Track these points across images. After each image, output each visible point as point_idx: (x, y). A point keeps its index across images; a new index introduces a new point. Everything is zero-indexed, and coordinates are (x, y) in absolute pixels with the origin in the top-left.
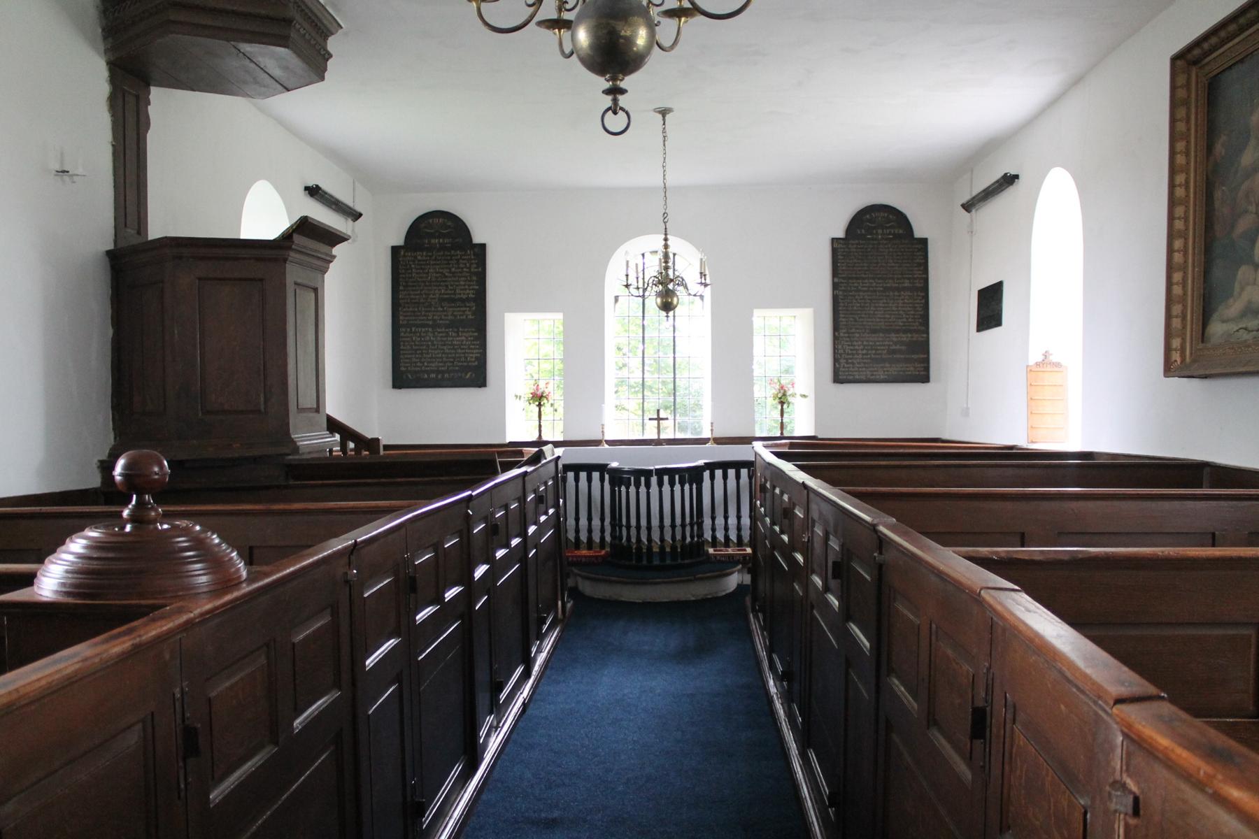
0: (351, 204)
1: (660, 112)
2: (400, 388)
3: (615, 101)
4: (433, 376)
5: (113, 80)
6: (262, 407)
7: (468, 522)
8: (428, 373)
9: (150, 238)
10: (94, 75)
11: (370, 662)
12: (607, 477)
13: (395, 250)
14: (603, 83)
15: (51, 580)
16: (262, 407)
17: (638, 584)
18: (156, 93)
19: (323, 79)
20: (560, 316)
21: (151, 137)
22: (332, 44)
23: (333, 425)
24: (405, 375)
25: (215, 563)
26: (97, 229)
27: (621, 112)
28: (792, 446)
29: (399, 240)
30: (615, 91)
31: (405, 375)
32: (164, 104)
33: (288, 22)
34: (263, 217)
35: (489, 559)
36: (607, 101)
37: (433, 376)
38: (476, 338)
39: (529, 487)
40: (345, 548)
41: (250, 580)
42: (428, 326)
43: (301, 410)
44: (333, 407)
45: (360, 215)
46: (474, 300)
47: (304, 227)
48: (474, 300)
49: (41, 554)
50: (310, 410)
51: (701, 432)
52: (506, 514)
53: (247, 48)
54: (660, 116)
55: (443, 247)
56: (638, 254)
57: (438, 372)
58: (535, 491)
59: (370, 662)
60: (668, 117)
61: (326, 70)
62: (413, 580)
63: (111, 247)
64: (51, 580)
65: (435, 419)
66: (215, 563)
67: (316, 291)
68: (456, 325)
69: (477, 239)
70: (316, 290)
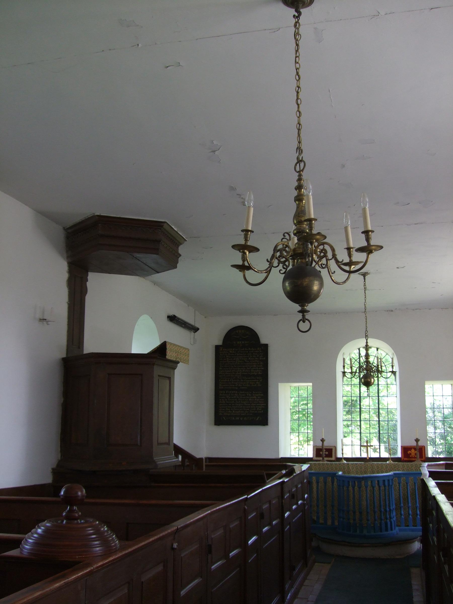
0: (192, 323)
1: (362, 275)
3: (303, 316)
4: (238, 418)
5: (70, 271)
6: (139, 444)
7: (246, 513)
9: (84, 353)
10: (60, 269)
11: (183, 592)
12: (336, 480)
13: (217, 347)
14: (297, 307)
15: (29, 542)
16: (139, 444)
18: (91, 276)
19: (176, 267)
20: (311, 384)
21: (88, 298)
22: (181, 250)
23: (178, 450)
24: (222, 418)
25: (105, 542)
26: (60, 351)
27: (306, 321)
28: (447, 466)
29: (219, 342)
30: (303, 311)
31: (222, 418)
32: (96, 282)
33: (159, 241)
34: (142, 343)
35: (258, 532)
36: (300, 316)
37: (238, 418)
39: (286, 489)
40: (172, 532)
41: (122, 548)
43: (159, 444)
44: (177, 440)
45: (198, 329)
47: (161, 350)
49: (27, 529)
50: (165, 444)
51: (395, 453)
52: (297, 490)
53: (138, 255)
54: (362, 277)
56: (351, 353)
58: (289, 492)
59: (183, 592)
60: (366, 277)
61: (178, 263)
62: (210, 547)
63: (64, 356)
64: (29, 542)
65: (239, 443)
66: (105, 542)
67: (170, 379)
70: (169, 378)
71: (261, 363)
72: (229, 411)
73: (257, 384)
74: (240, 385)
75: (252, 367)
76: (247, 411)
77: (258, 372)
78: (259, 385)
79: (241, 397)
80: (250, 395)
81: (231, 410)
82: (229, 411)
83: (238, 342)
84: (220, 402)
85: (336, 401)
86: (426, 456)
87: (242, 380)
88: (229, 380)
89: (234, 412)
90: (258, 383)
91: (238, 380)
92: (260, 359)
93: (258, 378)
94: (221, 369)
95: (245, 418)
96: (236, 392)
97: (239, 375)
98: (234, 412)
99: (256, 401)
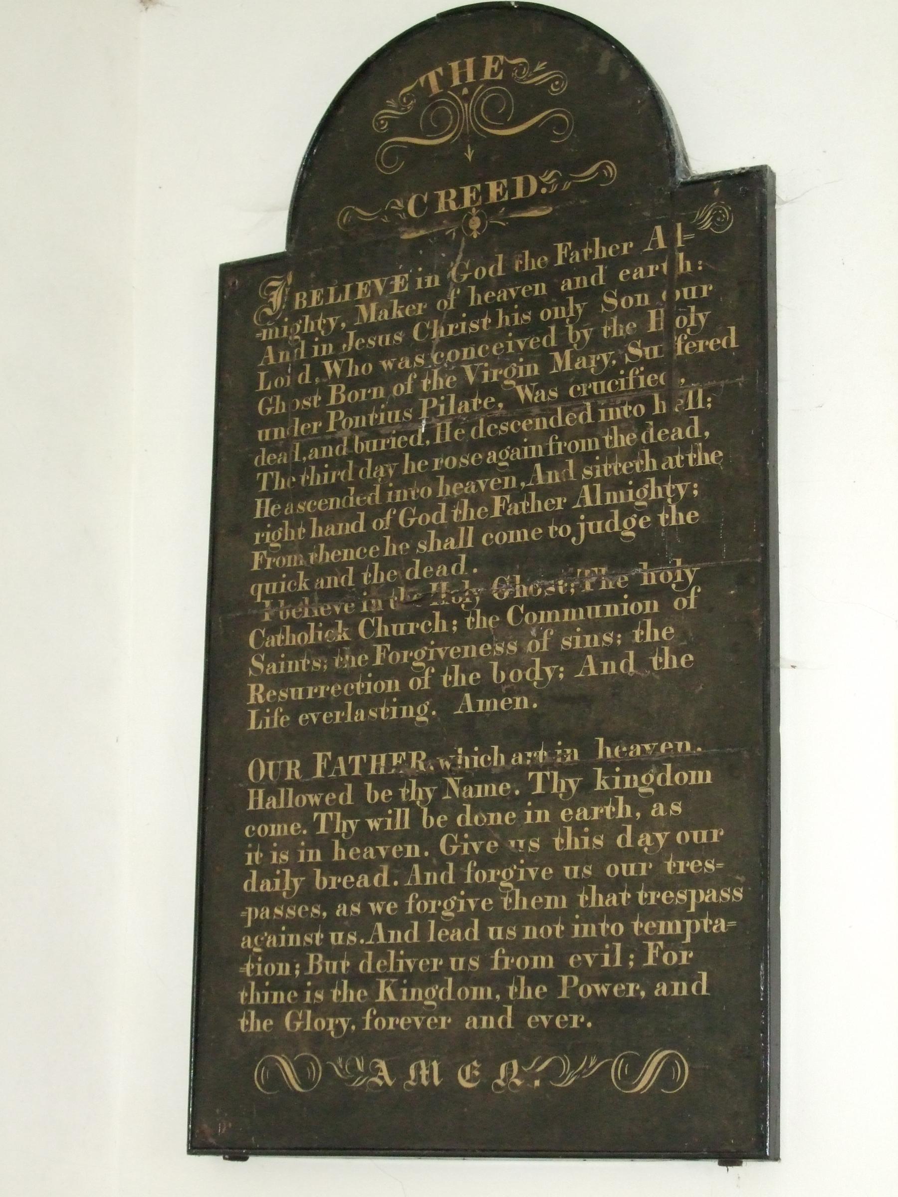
2: (236, 1152)
8: (400, 1049)
13: (240, 283)
17: (481, 1156)
37: (425, 1072)
38: (699, 807)
42: (400, 736)
46: (695, 543)
48: (695, 543)
55: (507, 230)
57: (456, 1047)
68: (571, 717)
69: (708, 146)
71: (694, 397)
72: (346, 994)
73: (645, 652)
74: (457, 678)
75: (588, 458)
76: (534, 977)
77: (656, 506)
78: (666, 660)
79: (467, 818)
80: (561, 785)
81: (357, 979)
82: (346, 994)
83: (446, 202)
84: (251, 885)
85: (779, 915)
86: (687, 172)
87: (480, 621)
88: (341, 634)
89: (385, 992)
90: (650, 633)
91: (440, 625)
92: (681, 347)
93: (649, 577)
94: (265, 508)
95: (510, 1074)
96: (418, 760)
97: (450, 558)
98: (385, 992)
99: (635, 854)
